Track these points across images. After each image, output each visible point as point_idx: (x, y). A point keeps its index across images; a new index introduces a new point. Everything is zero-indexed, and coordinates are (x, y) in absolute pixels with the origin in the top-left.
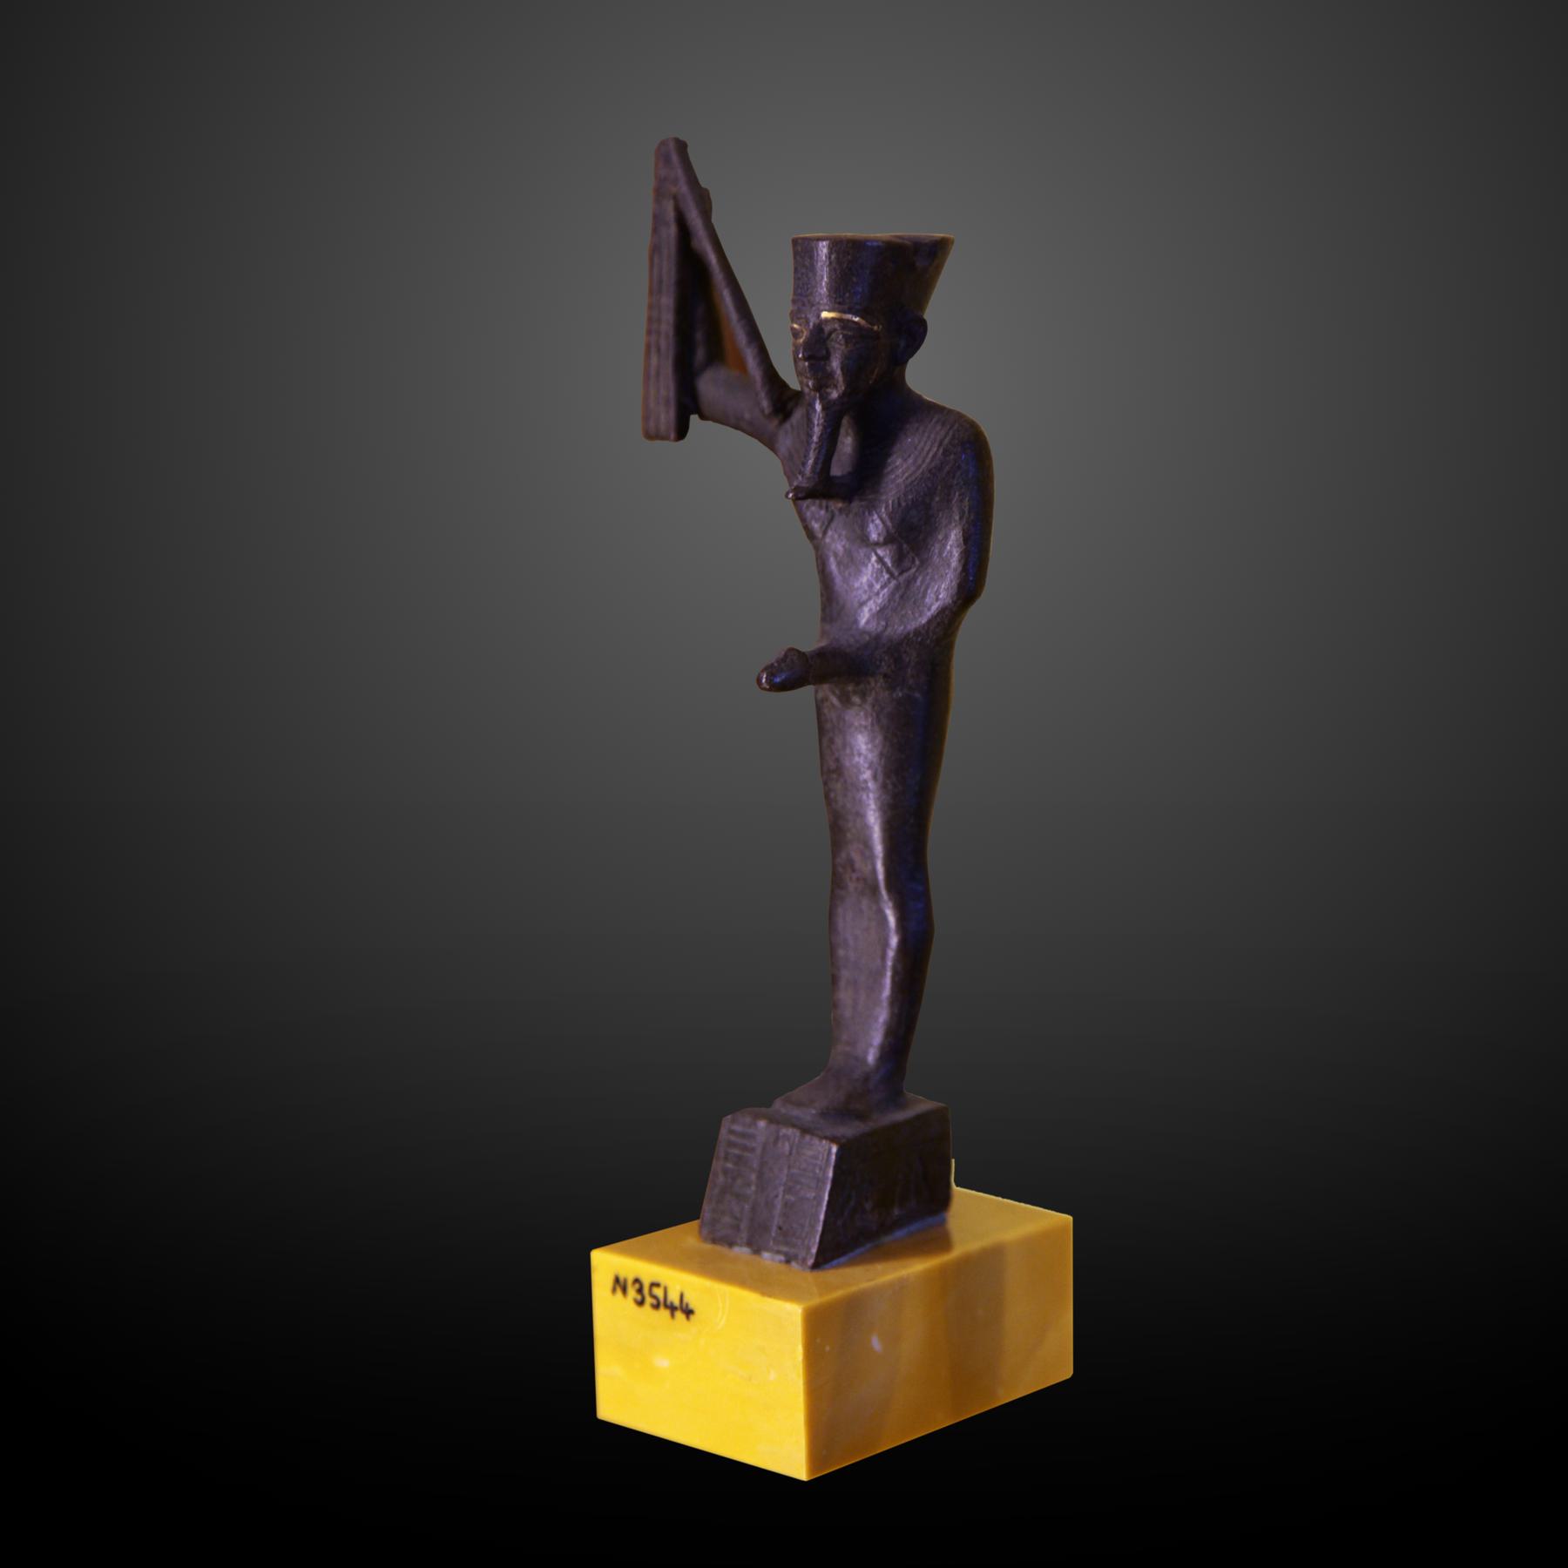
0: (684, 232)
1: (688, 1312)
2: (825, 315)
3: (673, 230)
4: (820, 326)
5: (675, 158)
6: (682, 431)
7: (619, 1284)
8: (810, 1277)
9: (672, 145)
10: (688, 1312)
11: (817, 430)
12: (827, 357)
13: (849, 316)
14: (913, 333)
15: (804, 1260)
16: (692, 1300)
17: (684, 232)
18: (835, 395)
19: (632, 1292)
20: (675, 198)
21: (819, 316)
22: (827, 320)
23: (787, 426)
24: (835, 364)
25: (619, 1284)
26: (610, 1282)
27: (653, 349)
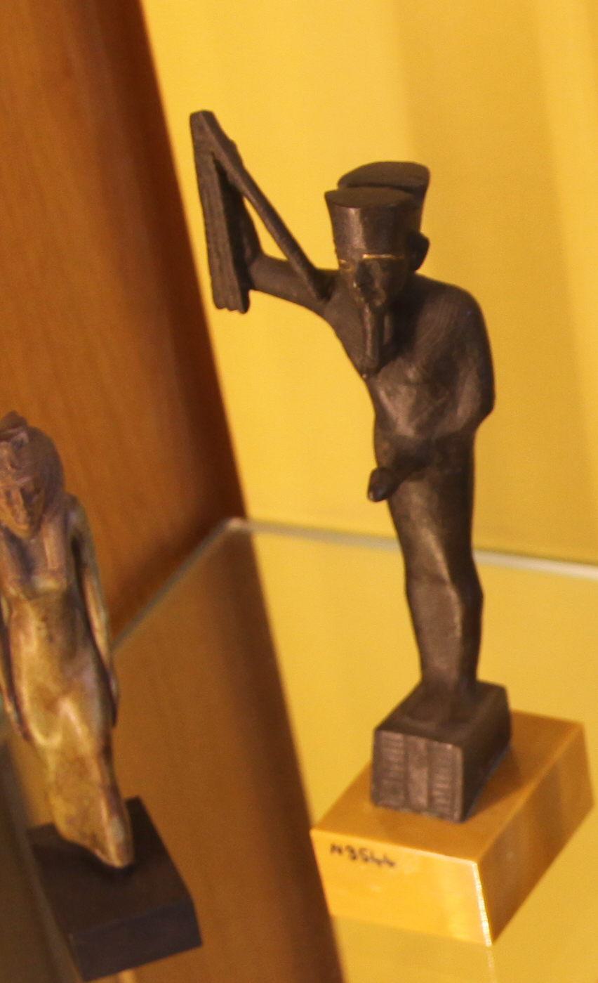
0: (222, 173)
1: (391, 864)
2: (365, 256)
3: (215, 176)
4: (363, 264)
5: (207, 129)
6: (245, 306)
7: (336, 849)
8: (462, 828)
9: (202, 118)
10: (391, 864)
11: (369, 328)
12: (372, 282)
13: (383, 256)
14: (419, 247)
15: (451, 817)
16: (392, 857)
17: (222, 173)
18: (378, 303)
19: (346, 854)
20: (213, 154)
21: (361, 257)
22: (367, 260)
23: (330, 304)
24: (377, 285)
25: (336, 849)
26: (328, 847)
27: (215, 255)
